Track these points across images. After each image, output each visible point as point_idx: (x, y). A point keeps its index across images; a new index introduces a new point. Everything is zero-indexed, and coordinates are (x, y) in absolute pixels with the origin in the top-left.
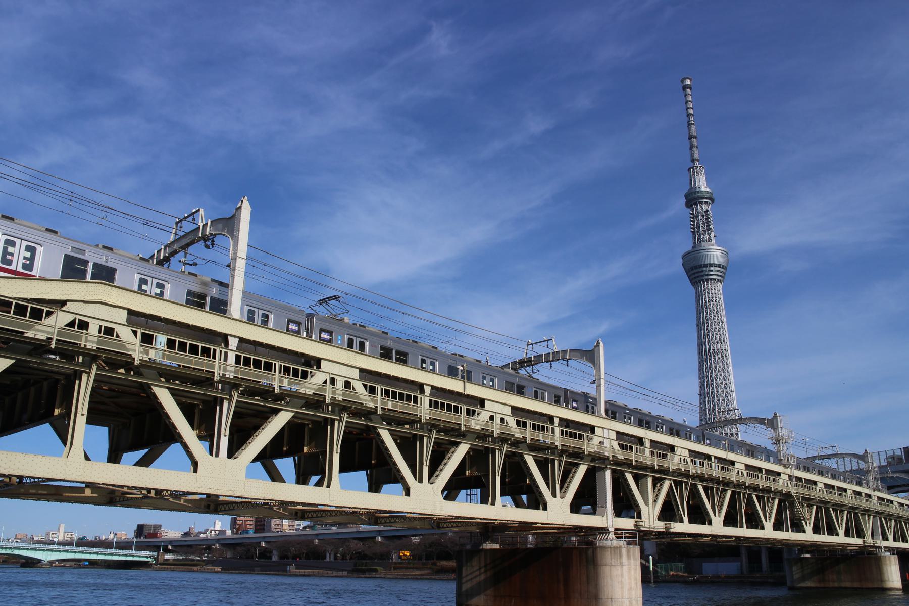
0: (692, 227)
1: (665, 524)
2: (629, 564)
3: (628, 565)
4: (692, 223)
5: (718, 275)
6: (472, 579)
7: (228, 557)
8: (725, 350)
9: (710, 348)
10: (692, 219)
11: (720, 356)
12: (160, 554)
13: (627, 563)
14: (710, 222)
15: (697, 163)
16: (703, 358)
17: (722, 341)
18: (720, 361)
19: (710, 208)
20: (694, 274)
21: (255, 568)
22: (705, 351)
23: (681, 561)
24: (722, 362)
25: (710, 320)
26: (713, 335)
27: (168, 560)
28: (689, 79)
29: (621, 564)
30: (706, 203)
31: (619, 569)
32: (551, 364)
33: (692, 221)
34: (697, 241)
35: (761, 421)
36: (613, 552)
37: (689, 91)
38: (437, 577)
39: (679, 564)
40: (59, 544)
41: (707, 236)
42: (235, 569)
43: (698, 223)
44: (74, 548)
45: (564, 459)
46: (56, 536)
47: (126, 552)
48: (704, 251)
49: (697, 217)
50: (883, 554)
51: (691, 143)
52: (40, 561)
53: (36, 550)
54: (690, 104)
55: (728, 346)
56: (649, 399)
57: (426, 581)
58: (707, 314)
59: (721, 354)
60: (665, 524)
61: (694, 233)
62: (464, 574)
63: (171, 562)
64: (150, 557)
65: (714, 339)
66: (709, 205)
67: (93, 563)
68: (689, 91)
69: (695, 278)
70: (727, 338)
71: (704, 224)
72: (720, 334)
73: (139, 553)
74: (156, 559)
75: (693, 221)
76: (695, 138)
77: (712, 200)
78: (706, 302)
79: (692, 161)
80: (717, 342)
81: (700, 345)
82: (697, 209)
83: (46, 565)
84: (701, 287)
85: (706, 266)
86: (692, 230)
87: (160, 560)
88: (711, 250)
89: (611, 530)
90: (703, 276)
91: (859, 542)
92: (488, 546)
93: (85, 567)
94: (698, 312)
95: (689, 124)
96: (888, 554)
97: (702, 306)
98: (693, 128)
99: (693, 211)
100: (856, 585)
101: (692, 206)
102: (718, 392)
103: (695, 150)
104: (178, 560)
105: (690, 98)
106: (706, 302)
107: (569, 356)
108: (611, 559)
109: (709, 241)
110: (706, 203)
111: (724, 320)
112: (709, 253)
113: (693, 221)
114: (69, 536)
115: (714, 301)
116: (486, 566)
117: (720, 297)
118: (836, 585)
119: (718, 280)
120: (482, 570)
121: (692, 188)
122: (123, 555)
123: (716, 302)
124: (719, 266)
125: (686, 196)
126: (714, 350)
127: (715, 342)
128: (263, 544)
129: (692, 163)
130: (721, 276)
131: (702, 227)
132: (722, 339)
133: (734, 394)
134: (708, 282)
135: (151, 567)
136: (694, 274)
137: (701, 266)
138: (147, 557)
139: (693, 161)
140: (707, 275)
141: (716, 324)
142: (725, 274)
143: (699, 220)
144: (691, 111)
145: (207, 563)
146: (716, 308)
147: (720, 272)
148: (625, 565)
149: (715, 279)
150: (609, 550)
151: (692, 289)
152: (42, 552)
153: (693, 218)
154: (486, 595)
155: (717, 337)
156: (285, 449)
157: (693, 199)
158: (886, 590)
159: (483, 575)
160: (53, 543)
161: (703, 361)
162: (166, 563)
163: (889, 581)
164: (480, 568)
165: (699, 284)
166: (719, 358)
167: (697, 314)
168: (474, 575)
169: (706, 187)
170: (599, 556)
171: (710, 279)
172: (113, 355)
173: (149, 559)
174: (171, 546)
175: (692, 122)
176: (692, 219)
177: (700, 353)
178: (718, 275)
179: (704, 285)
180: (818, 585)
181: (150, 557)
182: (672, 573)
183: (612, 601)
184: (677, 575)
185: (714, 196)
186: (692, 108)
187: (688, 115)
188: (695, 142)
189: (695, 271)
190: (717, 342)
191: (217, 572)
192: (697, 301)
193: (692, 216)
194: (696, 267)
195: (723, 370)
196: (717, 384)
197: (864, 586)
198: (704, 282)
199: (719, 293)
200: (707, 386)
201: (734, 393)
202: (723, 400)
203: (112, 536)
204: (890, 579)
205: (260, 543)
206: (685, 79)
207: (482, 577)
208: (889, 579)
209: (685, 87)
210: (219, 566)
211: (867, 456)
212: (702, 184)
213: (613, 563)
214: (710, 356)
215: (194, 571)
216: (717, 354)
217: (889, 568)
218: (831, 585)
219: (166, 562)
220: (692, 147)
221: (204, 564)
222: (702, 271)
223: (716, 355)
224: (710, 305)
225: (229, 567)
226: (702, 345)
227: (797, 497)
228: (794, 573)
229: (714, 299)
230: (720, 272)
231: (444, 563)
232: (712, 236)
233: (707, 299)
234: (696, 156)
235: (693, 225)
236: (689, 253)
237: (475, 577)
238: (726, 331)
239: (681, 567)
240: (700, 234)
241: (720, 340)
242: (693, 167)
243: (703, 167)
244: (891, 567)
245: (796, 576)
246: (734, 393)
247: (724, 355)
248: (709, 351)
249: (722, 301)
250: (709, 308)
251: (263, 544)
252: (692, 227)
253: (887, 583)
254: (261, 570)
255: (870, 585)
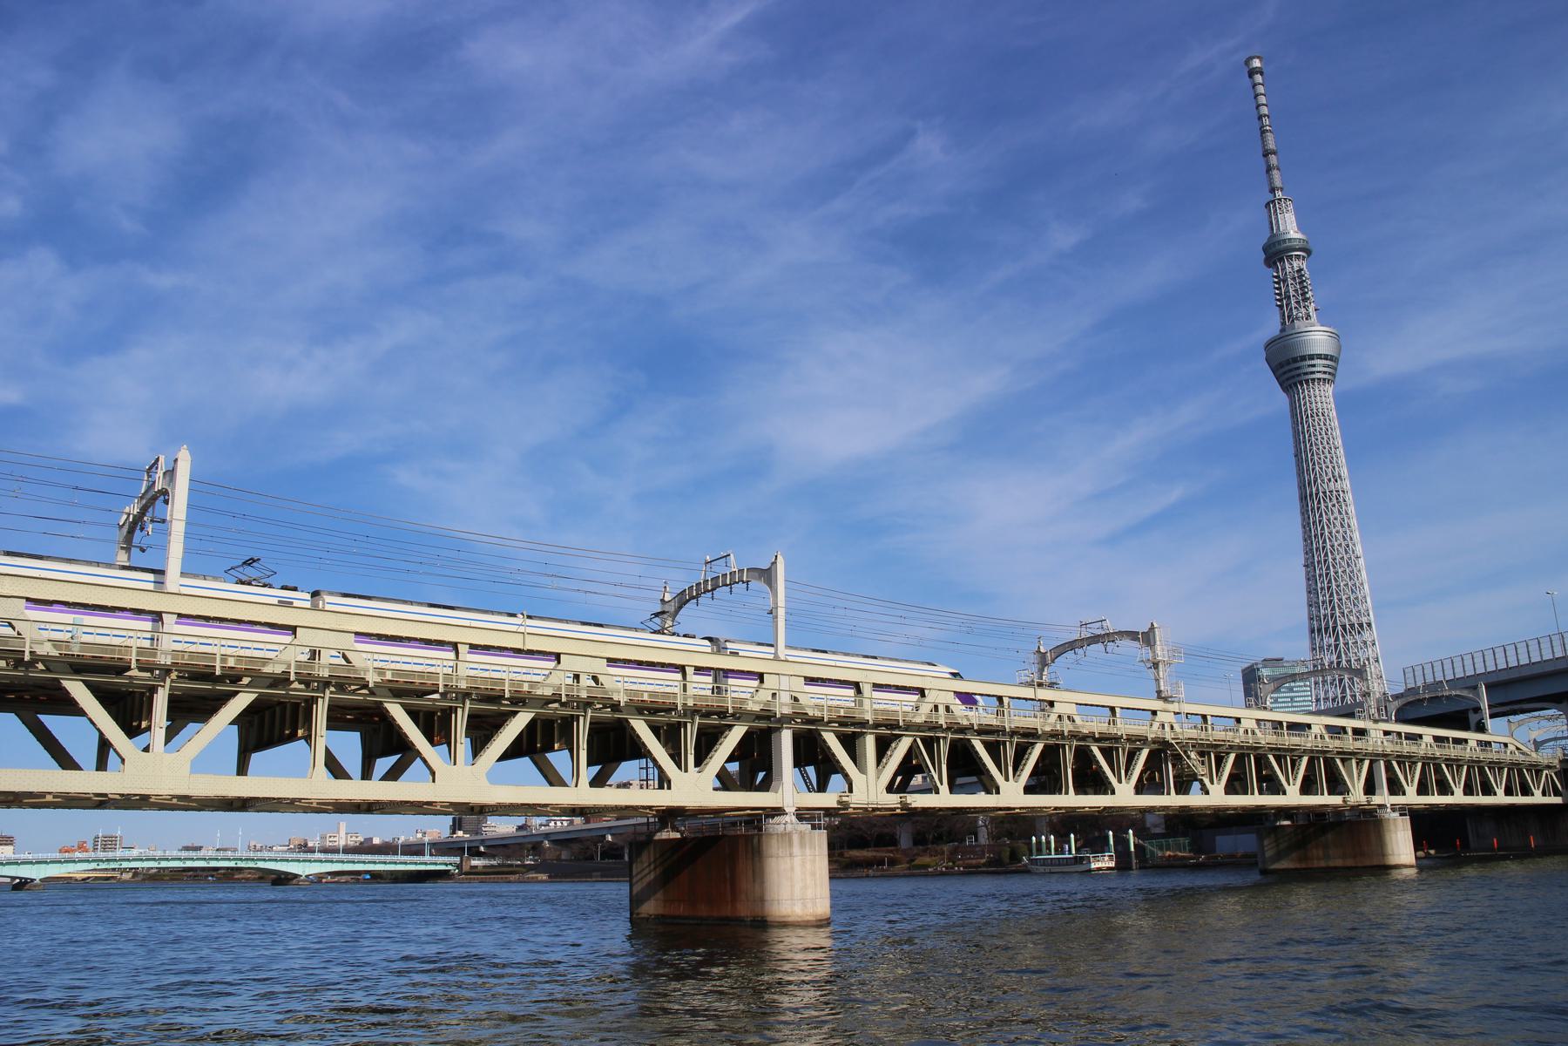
0: (1278, 297)
1: (901, 798)
2: (803, 855)
3: (802, 856)
4: (1277, 292)
5: (1325, 373)
6: (642, 879)
7: (563, 857)
8: (1343, 491)
9: (1317, 489)
10: (1277, 286)
11: (1335, 501)
12: (464, 858)
13: (799, 854)
14: (1306, 287)
15: (1279, 194)
16: (1307, 505)
17: (1337, 478)
18: (1336, 510)
19: (1304, 264)
20: (1285, 373)
21: (594, 874)
22: (1311, 495)
23: (1184, 835)
24: (1339, 511)
25: (1316, 444)
26: (1321, 468)
27: (477, 867)
28: (1258, 57)
29: (791, 855)
30: (1298, 257)
31: (788, 861)
32: (731, 588)
33: (1277, 289)
34: (1288, 320)
35: (1133, 635)
36: (780, 839)
37: (1258, 78)
38: (842, 875)
39: (1181, 840)
40: (347, 850)
41: (1303, 310)
42: (566, 876)
43: (1287, 291)
44: (341, 856)
45: (697, 720)
46: (335, 839)
47: (415, 858)
48: (1298, 335)
49: (1285, 281)
50: (1387, 816)
51: (1267, 162)
52: (296, 876)
53: (287, 861)
54: (1263, 100)
55: (1347, 485)
56: (907, 621)
57: (903, 879)
58: (1310, 436)
59: (1337, 499)
60: (901, 798)
61: (1281, 307)
62: (634, 873)
63: (480, 869)
64: (451, 864)
65: (1324, 474)
66: (1303, 260)
67: (376, 876)
68: (1258, 78)
69: (1288, 379)
70: (1344, 472)
71: (1296, 291)
72: (1334, 467)
73: (434, 859)
74: (459, 866)
75: (1279, 289)
76: (1274, 153)
77: (1308, 252)
78: (1307, 417)
79: (1270, 192)
80: (1330, 480)
81: (1302, 486)
82: (1284, 269)
83: (302, 881)
84: (1298, 394)
85: (1303, 358)
86: (1279, 303)
87: (466, 868)
88: (1313, 333)
89: (790, 809)
90: (1299, 375)
91: (1336, 800)
92: (665, 835)
93: (366, 881)
94: (1296, 433)
95: (1263, 132)
96: (1396, 814)
97: (1302, 423)
98: (1270, 138)
99: (1278, 272)
100: (1350, 862)
101: (1275, 263)
102: (1334, 559)
103: (1275, 172)
104: (492, 866)
105: (1261, 89)
106: (1307, 417)
107: (747, 577)
108: (778, 849)
109: (1307, 319)
110: (1298, 257)
111: (1339, 442)
112: (1313, 337)
113: (1279, 289)
114: (354, 839)
115: (1320, 414)
116: (655, 861)
117: (1329, 407)
118: (1323, 864)
119: (1324, 379)
120: (652, 867)
121: (1273, 235)
122: (410, 863)
123: (1323, 415)
124: (1326, 357)
125: (1265, 249)
126: (1324, 493)
127: (1326, 480)
128: (609, 838)
129: (1272, 195)
130: (1330, 373)
131: (1294, 296)
132: (1336, 474)
133: (1361, 561)
134: (1308, 385)
135: (451, 879)
136: (1285, 373)
137: (1295, 360)
138: (446, 865)
139: (1273, 190)
140: (1306, 374)
141: (1326, 451)
142: (1335, 369)
143: (1288, 285)
144: (1264, 110)
145: (530, 868)
146: (1325, 425)
147: (1328, 366)
148: (797, 856)
149: (1319, 379)
150: (775, 837)
151: (1282, 398)
152: (296, 863)
153: (1278, 283)
154: (656, 900)
155: (1329, 471)
156: (287, 732)
157: (1276, 252)
158: (1387, 868)
159: (652, 873)
160: (335, 851)
161: (1308, 511)
162: (474, 871)
163: (1393, 855)
164: (649, 865)
165: (1294, 389)
166: (1334, 506)
167: (1294, 437)
168: (643, 874)
169: (1296, 232)
170: (764, 844)
171: (1312, 379)
172: (4, 653)
173: (450, 867)
174: (485, 847)
175: (1268, 128)
176: (1277, 286)
177: (1303, 498)
178: (1325, 373)
179: (1304, 390)
180: (1298, 866)
181: (451, 864)
182: (1168, 853)
183: (779, 903)
184: (1175, 856)
185: (1311, 246)
186: (1266, 106)
187: (1260, 117)
188: (1273, 159)
189: (1287, 368)
190: (1330, 480)
191: (542, 882)
192: (1292, 417)
193: (1276, 280)
194: (1288, 363)
195: (1341, 524)
196: (1332, 546)
197: (1360, 865)
198: (1302, 385)
199: (1328, 401)
200: (1317, 551)
201: (1362, 559)
202: (1344, 572)
203: (419, 835)
204: (1395, 853)
205: (605, 836)
206: (1251, 58)
207: (652, 876)
208: (1393, 851)
209: (1252, 73)
210: (545, 873)
211: (1366, 671)
212: (1290, 227)
213: (780, 855)
214: (1319, 502)
215: (509, 882)
216: (1330, 499)
217: (1393, 836)
218: (1316, 864)
219: (473, 871)
220: (1269, 169)
221: (524, 870)
222: (1298, 368)
223: (1328, 500)
224: (1314, 420)
225: (558, 872)
226: (1305, 485)
227: (1181, 745)
228: (1266, 849)
229: (1320, 410)
230: (1328, 366)
231: (855, 853)
232: (1310, 310)
233: (1309, 412)
234: (1278, 183)
235: (1280, 294)
236: (1275, 340)
237: (645, 876)
238: (1344, 461)
239: (1184, 843)
240: (1291, 308)
241: (1334, 477)
242: (1273, 201)
243: (1290, 200)
244: (1396, 834)
245: (1269, 854)
246: (1362, 559)
247: (1341, 500)
248: (1317, 494)
249: (1333, 414)
250: (1313, 426)
251: (609, 838)
252: (1278, 297)
253: (1391, 857)
254: (602, 876)
255: (1368, 863)
